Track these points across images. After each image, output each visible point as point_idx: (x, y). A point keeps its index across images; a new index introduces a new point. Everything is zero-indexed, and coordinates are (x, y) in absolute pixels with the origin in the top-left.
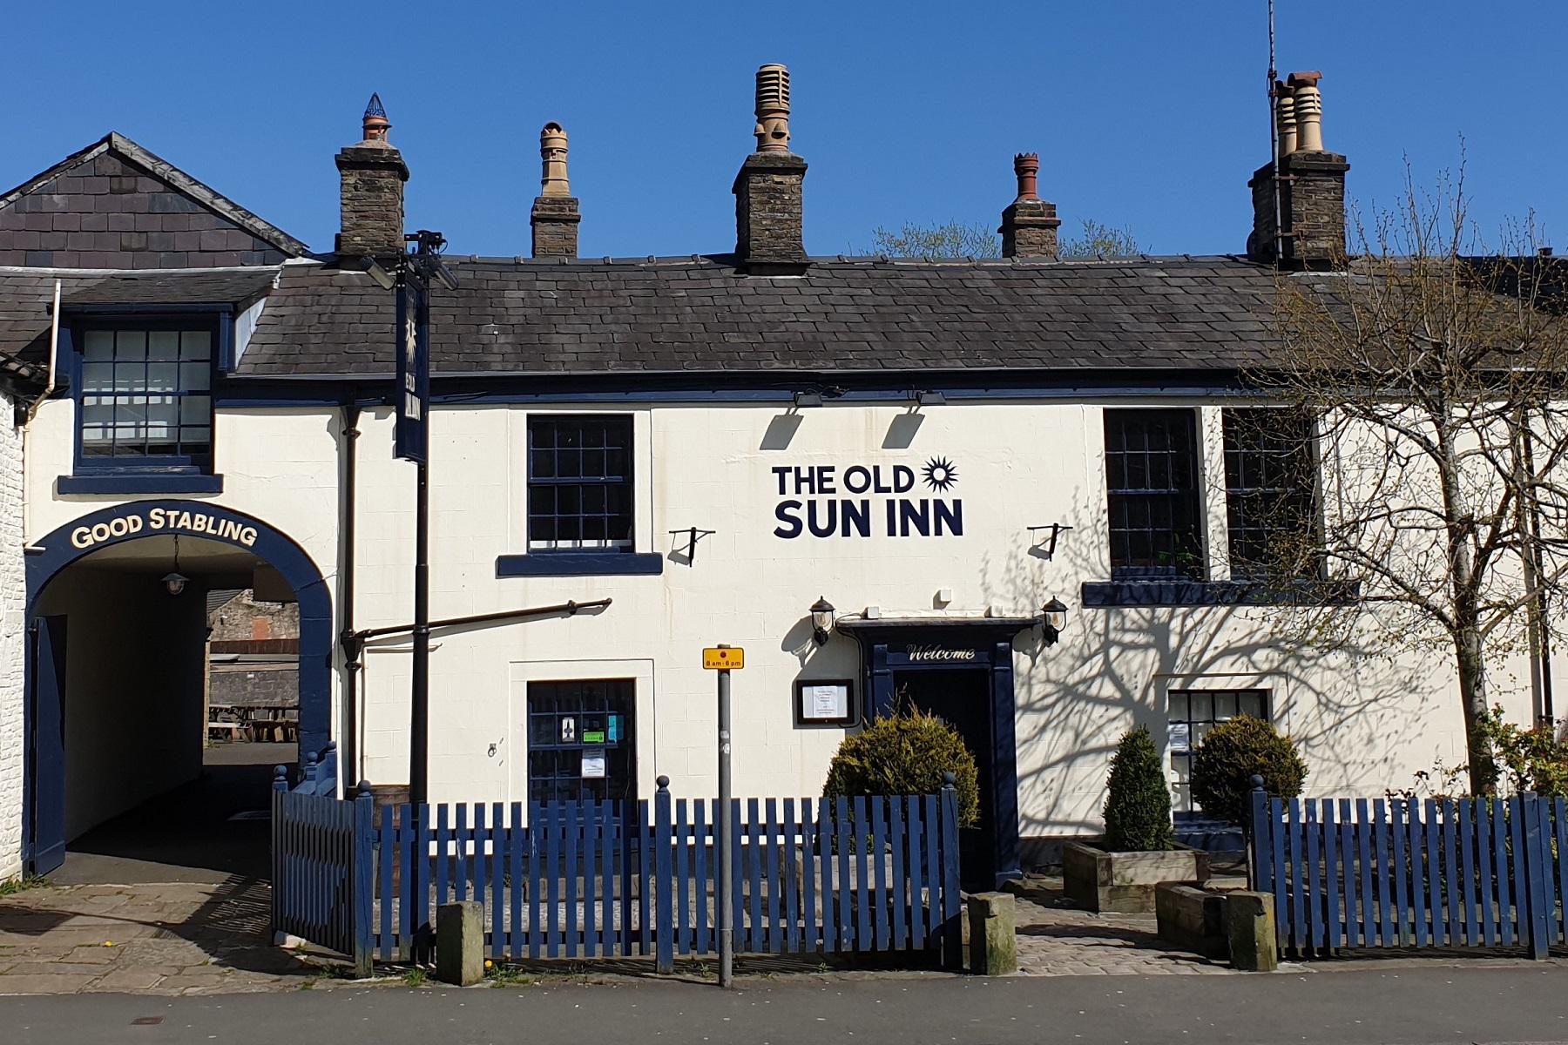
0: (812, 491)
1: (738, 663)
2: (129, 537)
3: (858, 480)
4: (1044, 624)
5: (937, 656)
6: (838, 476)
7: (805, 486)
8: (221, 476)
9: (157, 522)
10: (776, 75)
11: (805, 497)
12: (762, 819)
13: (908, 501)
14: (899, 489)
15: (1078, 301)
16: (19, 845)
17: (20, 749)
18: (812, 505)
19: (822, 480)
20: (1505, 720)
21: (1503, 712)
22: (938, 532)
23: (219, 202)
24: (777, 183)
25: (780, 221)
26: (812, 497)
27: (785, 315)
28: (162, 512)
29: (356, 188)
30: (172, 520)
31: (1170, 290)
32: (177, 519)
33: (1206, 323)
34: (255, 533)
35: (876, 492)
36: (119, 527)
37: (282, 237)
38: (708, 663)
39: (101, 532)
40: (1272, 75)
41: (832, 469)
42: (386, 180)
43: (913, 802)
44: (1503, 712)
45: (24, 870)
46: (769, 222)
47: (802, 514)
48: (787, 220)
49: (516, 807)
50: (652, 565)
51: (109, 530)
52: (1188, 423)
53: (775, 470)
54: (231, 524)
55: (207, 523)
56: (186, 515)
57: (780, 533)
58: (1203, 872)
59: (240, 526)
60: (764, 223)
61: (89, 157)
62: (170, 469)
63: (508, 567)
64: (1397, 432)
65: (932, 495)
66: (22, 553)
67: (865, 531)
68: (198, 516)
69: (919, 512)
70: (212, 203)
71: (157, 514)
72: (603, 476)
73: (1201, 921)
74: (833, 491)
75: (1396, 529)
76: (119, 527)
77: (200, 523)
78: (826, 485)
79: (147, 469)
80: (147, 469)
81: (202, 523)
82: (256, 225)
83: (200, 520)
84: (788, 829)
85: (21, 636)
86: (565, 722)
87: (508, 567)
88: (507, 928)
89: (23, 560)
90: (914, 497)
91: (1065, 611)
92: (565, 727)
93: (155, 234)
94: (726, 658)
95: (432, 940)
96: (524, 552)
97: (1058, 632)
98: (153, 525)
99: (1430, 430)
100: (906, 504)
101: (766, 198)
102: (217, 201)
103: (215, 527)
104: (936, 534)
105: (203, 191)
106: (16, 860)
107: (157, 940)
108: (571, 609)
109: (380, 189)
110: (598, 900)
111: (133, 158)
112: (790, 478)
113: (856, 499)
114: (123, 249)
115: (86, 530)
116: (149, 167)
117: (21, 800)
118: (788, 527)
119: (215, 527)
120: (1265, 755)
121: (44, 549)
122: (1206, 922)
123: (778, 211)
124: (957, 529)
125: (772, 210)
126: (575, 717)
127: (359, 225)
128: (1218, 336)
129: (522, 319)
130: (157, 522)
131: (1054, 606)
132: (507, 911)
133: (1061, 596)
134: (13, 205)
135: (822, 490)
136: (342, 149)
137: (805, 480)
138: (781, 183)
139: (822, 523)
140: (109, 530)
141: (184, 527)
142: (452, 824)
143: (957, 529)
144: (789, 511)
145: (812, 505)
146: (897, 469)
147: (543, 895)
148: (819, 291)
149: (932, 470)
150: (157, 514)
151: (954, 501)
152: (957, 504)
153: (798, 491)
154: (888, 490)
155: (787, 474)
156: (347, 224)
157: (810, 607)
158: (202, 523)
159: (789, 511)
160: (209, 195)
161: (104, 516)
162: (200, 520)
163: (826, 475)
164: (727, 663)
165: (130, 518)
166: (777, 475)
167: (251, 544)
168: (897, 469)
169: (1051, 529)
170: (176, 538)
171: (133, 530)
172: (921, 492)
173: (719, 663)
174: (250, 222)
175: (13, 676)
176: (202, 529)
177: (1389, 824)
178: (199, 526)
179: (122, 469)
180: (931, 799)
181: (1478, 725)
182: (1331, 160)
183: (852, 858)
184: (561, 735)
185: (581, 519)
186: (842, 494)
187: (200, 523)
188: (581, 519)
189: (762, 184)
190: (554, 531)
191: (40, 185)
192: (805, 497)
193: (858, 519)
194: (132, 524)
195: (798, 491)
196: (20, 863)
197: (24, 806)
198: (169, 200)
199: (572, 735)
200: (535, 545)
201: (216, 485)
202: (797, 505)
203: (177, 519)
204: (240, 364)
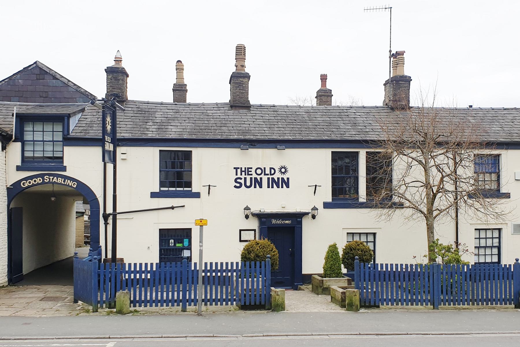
0: (245, 175)
1: (205, 224)
2: (38, 184)
3: (259, 171)
4: (311, 213)
5: (280, 222)
6: (253, 171)
7: (243, 173)
8: (66, 166)
9: (47, 180)
10: (242, 47)
11: (243, 176)
12: (219, 268)
13: (274, 178)
14: (271, 174)
15: (328, 119)
16: (7, 274)
17: (6, 246)
18: (245, 179)
19: (248, 171)
20: (440, 242)
21: (439, 240)
22: (282, 187)
23: (70, 83)
24: (241, 81)
25: (242, 93)
26: (245, 176)
27: (241, 122)
28: (48, 177)
29: (111, 79)
30: (51, 179)
31: (356, 116)
32: (53, 179)
33: (365, 126)
34: (76, 184)
35: (264, 175)
36: (35, 181)
37: (89, 94)
38: (197, 224)
39: (30, 183)
40: (390, 51)
41: (251, 168)
42: (120, 77)
43: (258, 263)
44: (439, 240)
45: (8, 281)
46: (238, 93)
47: (242, 181)
48: (244, 93)
49: (237, 263)
50: (197, 195)
51: (32, 182)
52: (356, 155)
53: (234, 168)
54: (69, 181)
55: (62, 180)
56: (55, 178)
57: (235, 187)
58: (234, 290)
59: (72, 181)
60: (237, 93)
61: (30, 68)
62: (50, 164)
63: (154, 195)
64: (412, 159)
65: (281, 176)
66: (6, 188)
67: (261, 187)
68: (59, 178)
69: (286, 181)
70: (68, 83)
71: (47, 177)
72: (183, 169)
73: (340, 297)
74: (252, 175)
75: (407, 187)
76: (35, 181)
77: (60, 180)
78: (250, 173)
79: (43, 164)
80: (43, 164)
81: (60, 180)
82: (81, 90)
83: (60, 179)
84: (232, 271)
85: (6, 213)
86: (171, 241)
87: (154, 195)
88: (154, 299)
89: (6, 190)
90: (275, 177)
91: (317, 210)
92: (171, 242)
93: (50, 93)
94: (202, 222)
95: (400, 287)
96: (158, 191)
97: (315, 216)
98: (45, 180)
99: (421, 158)
100: (273, 179)
101: (238, 86)
102: (69, 83)
103: (64, 182)
104: (282, 188)
105: (64, 79)
106: (5, 279)
107: (40, 302)
108: (173, 208)
109: (119, 80)
110: (181, 291)
111: (43, 69)
112: (239, 171)
113: (258, 177)
114: (41, 97)
115: (25, 182)
116: (48, 71)
117: (7, 261)
118: (238, 185)
119: (64, 182)
120: (361, 251)
121: (12, 187)
122: (342, 298)
123: (241, 90)
124: (288, 187)
125: (240, 89)
126: (174, 239)
127: (112, 91)
128: (367, 130)
129: (160, 121)
130: (47, 180)
131: (315, 209)
132: (149, 294)
133: (411, 214)
134: (6, 83)
135: (248, 175)
136: (107, 67)
137: (243, 171)
138: (242, 81)
139: (248, 184)
140: (32, 182)
141: (55, 181)
142: (224, 268)
143: (288, 187)
144: (238, 180)
145: (245, 179)
146: (271, 169)
147: (165, 290)
148: (252, 115)
149: (281, 169)
150: (47, 177)
151: (287, 178)
152: (288, 179)
153: (241, 175)
154: (268, 175)
155: (238, 169)
156: (108, 90)
157: (244, 208)
158: (60, 180)
159: (238, 180)
160: (67, 81)
161: (31, 178)
162: (60, 179)
163: (250, 170)
164: (202, 224)
165: (38, 179)
166: (235, 170)
167: (75, 187)
168: (271, 169)
169: (315, 187)
170: (53, 185)
171: (39, 182)
172: (277, 175)
173: (200, 224)
174: (79, 89)
175: (3, 225)
176: (60, 182)
177: (466, 272)
178: (59, 181)
179: (36, 164)
180: (263, 262)
181: (433, 245)
182: (406, 78)
183: (245, 279)
184: (169, 244)
185: (176, 182)
186: (254, 176)
187: (60, 180)
188: (176, 182)
189: (237, 81)
190: (346, 203)
191: (15, 77)
192: (243, 176)
193: (258, 183)
194: (39, 180)
195: (241, 175)
196: (7, 279)
197: (8, 262)
198: (54, 82)
199: (173, 244)
200: (162, 189)
201: (64, 169)
202: (241, 179)
203: (53, 179)
204: (72, 133)
